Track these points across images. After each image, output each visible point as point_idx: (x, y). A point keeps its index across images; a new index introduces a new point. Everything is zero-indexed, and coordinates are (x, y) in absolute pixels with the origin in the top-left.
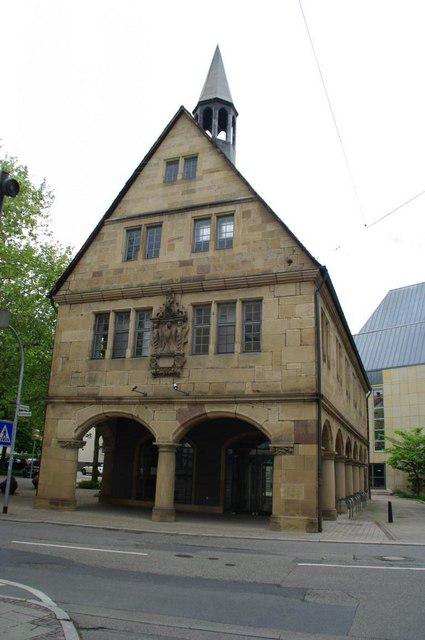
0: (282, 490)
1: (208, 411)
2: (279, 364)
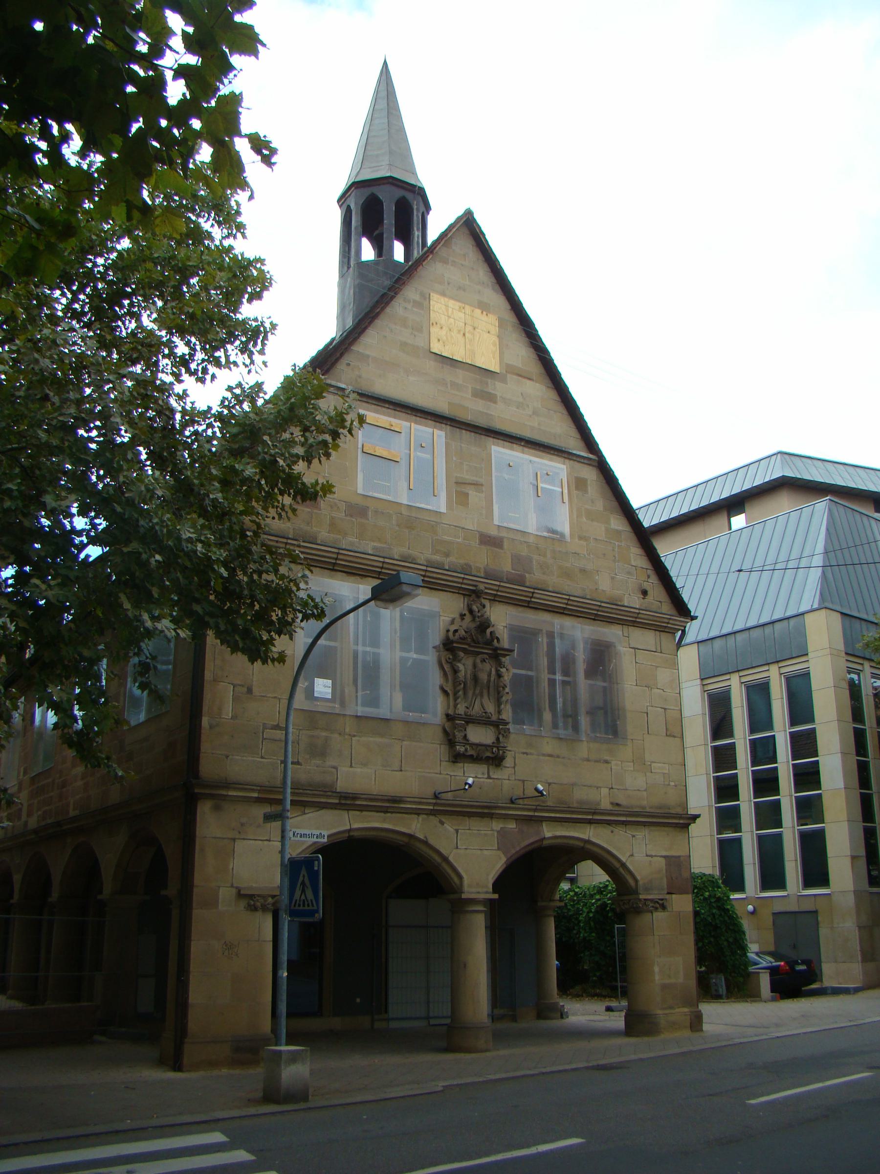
0: (656, 969)
1: (548, 834)
2: (641, 763)
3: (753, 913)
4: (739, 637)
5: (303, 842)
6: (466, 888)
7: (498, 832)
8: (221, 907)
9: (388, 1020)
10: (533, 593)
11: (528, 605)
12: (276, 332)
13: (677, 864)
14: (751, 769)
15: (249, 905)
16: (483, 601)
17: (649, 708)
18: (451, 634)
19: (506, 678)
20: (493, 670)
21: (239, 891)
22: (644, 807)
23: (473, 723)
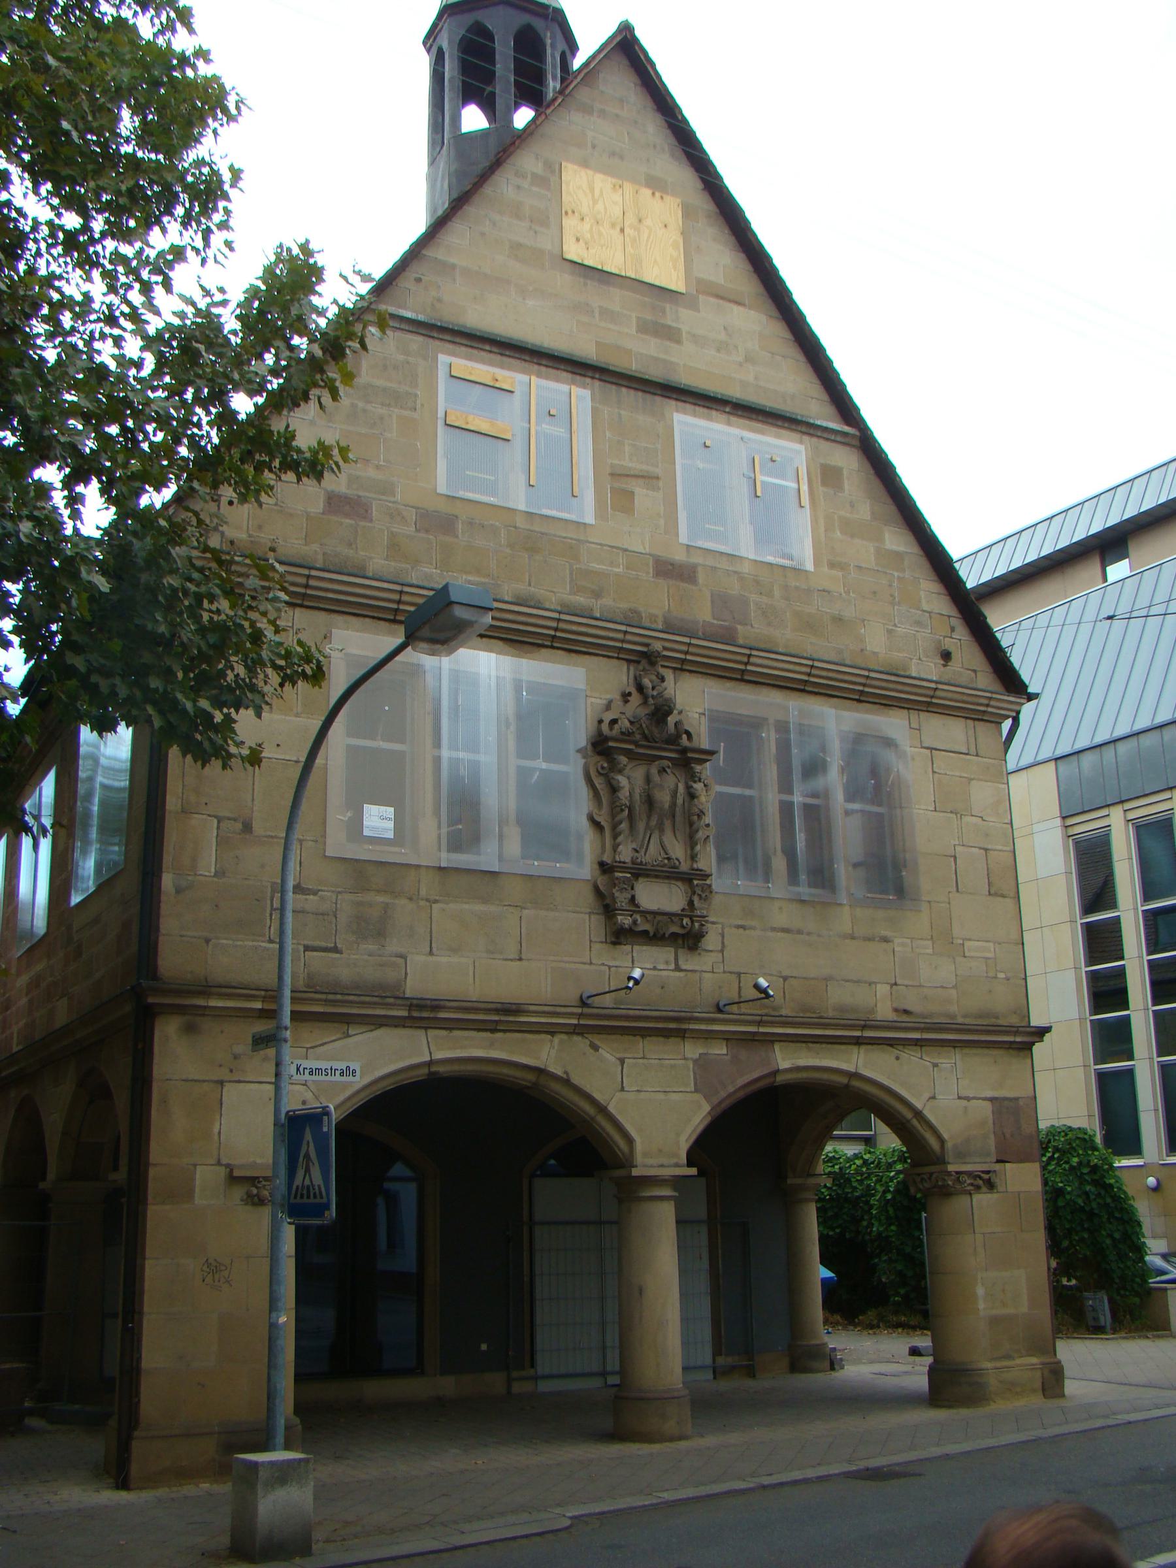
0: (980, 1291)
1: (784, 1064)
2: (947, 942)
3: (1156, 1189)
4: (1122, 747)
5: (345, 1086)
6: (639, 1158)
7: (695, 1061)
8: (198, 1200)
9: (536, 1378)
10: (749, 656)
11: (742, 677)
12: (241, 184)
13: (1013, 1112)
14: (1146, 958)
15: (249, 1196)
16: (662, 671)
17: (958, 849)
18: (605, 727)
19: (703, 799)
20: (681, 787)
21: (231, 1171)
22: (953, 1017)
23: (648, 876)
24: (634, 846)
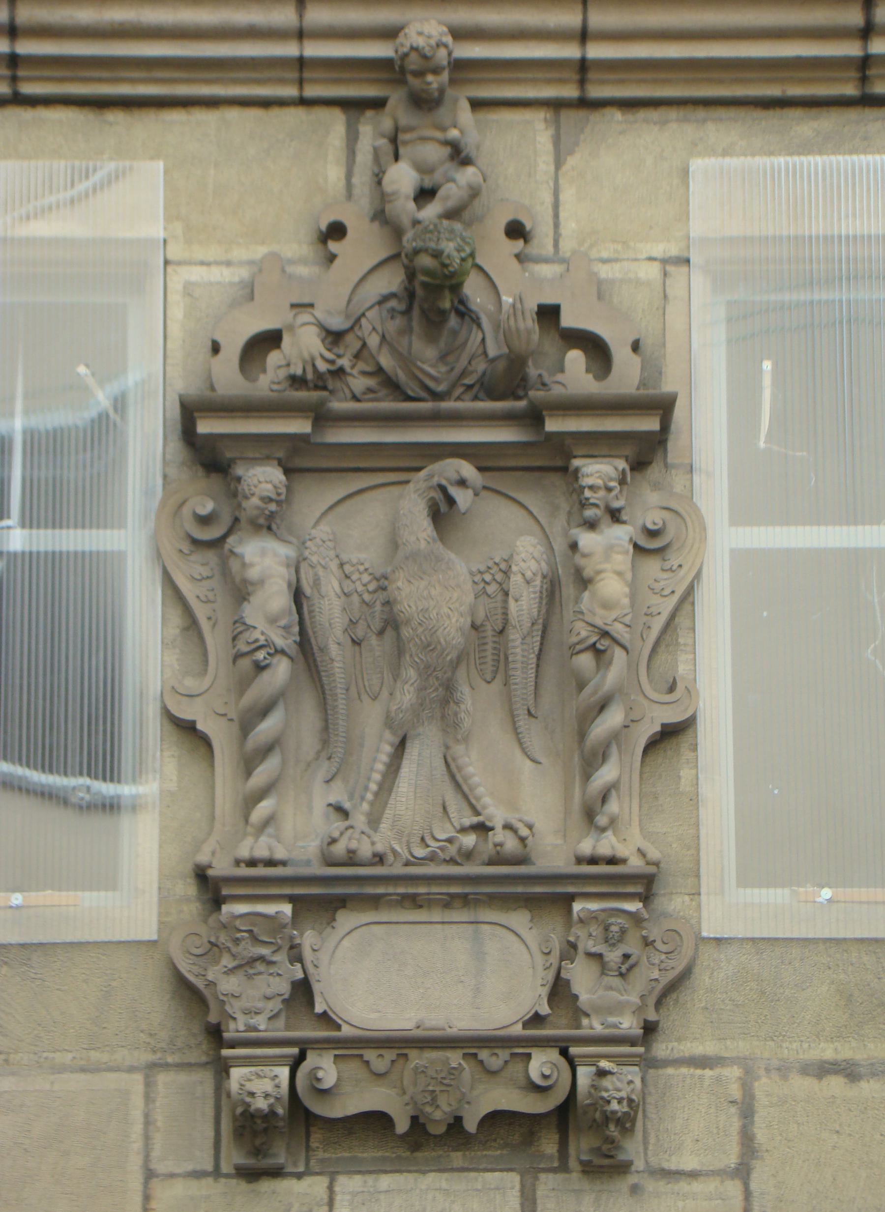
24: (337, 794)
